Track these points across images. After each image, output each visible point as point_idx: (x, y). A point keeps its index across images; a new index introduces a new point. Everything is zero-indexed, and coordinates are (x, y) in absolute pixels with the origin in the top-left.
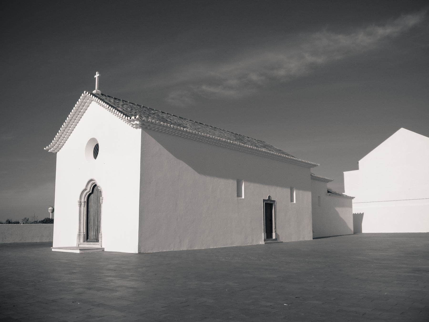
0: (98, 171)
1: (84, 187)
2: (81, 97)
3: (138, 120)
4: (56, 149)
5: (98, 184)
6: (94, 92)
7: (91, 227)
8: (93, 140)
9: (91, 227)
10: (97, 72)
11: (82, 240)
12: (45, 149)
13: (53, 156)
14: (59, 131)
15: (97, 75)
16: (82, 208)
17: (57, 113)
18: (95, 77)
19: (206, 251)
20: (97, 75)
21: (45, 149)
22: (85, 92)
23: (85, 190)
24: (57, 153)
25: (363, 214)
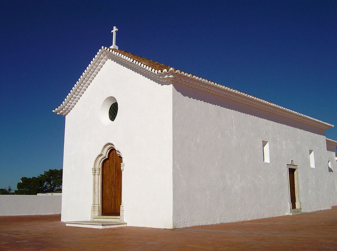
0: (117, 134)
1: (99, 153)
2: (98, 53)
3: (172, 73)
4: (65, 111)
5: (117, 148)
6: (111, 47)
7: (110, 201)
8: (112, 98)
9: (110, 201)
10: (114, 27)
11: (97, 214)
12: (53, 111)
13: (62, 119)
14: (79, 79)
15: (115, 29)
16: (97, 176)
17: (68, 71)
18: (112, 31)
19: (228, 223)
20: (115, 29)
21: (53, 111)
22: (103, 47)
23: (101, 155)
24: (65, 115)
25: (112, 151)
